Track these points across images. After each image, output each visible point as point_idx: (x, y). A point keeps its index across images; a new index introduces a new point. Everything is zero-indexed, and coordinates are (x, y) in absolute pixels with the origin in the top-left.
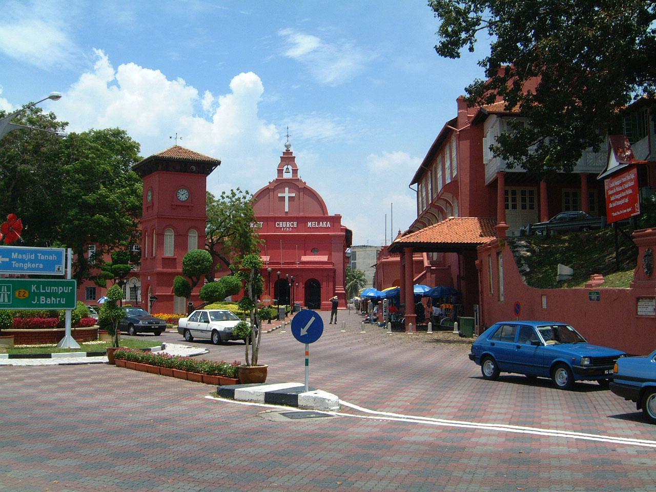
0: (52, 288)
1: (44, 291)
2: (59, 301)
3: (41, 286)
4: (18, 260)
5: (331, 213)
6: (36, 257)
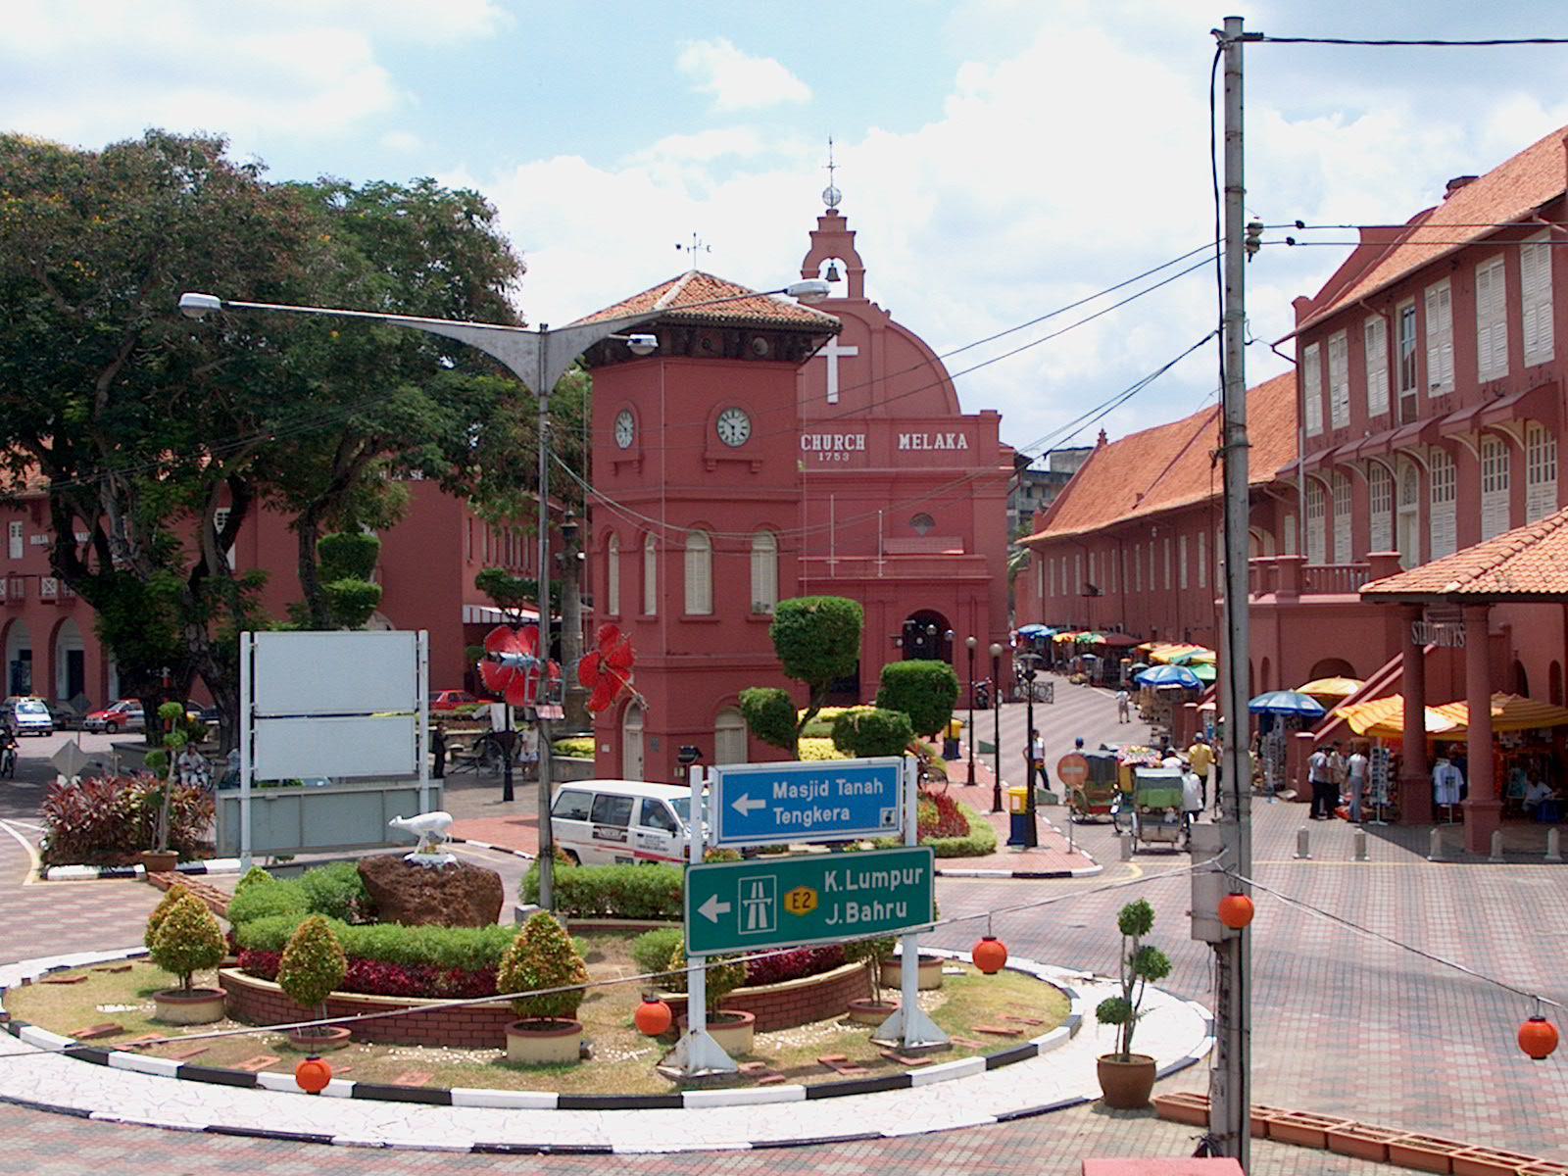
0: (875, 875)
1: (855, 887)
2: (893, 911)
3: (848, 872)
4: (789, 804)
5: (969, 407)
6: (834, 788)
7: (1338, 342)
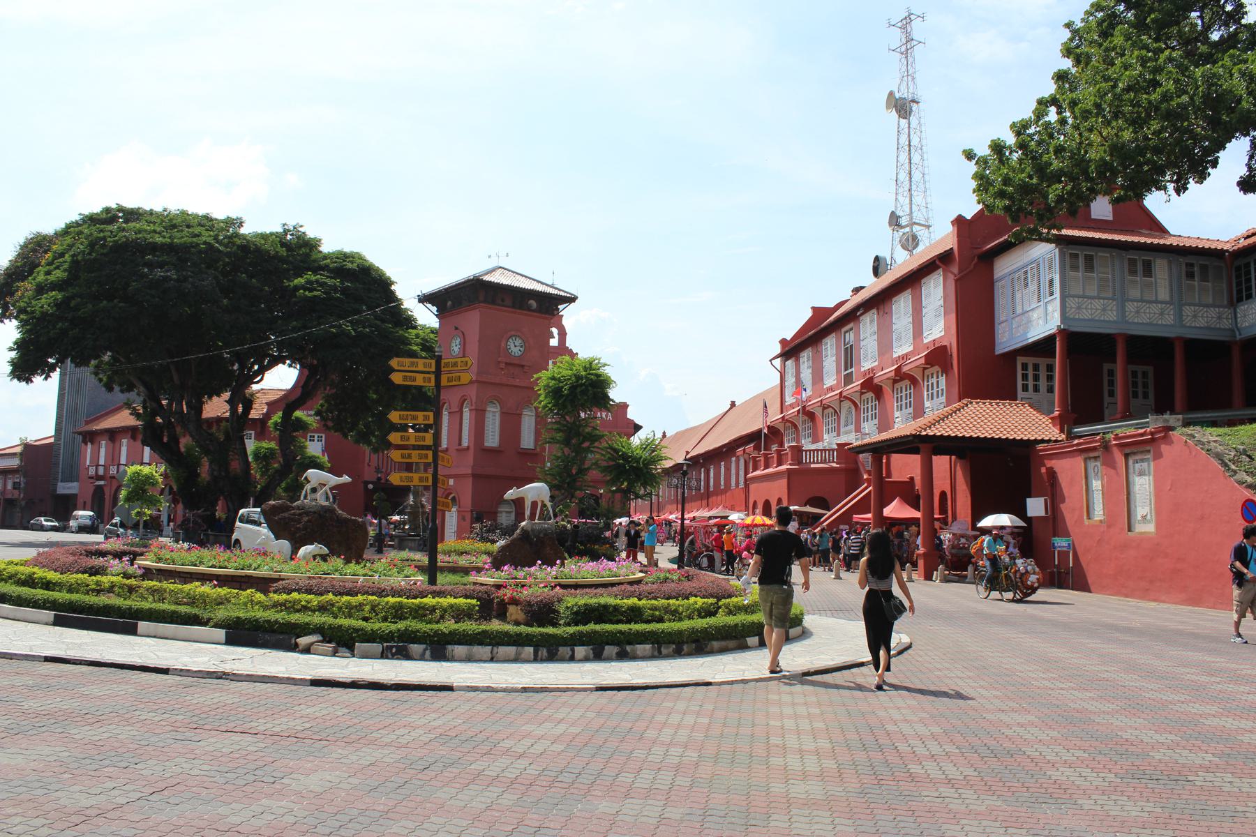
7: (806, 355)
